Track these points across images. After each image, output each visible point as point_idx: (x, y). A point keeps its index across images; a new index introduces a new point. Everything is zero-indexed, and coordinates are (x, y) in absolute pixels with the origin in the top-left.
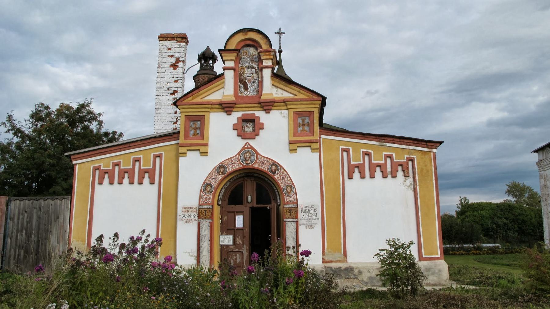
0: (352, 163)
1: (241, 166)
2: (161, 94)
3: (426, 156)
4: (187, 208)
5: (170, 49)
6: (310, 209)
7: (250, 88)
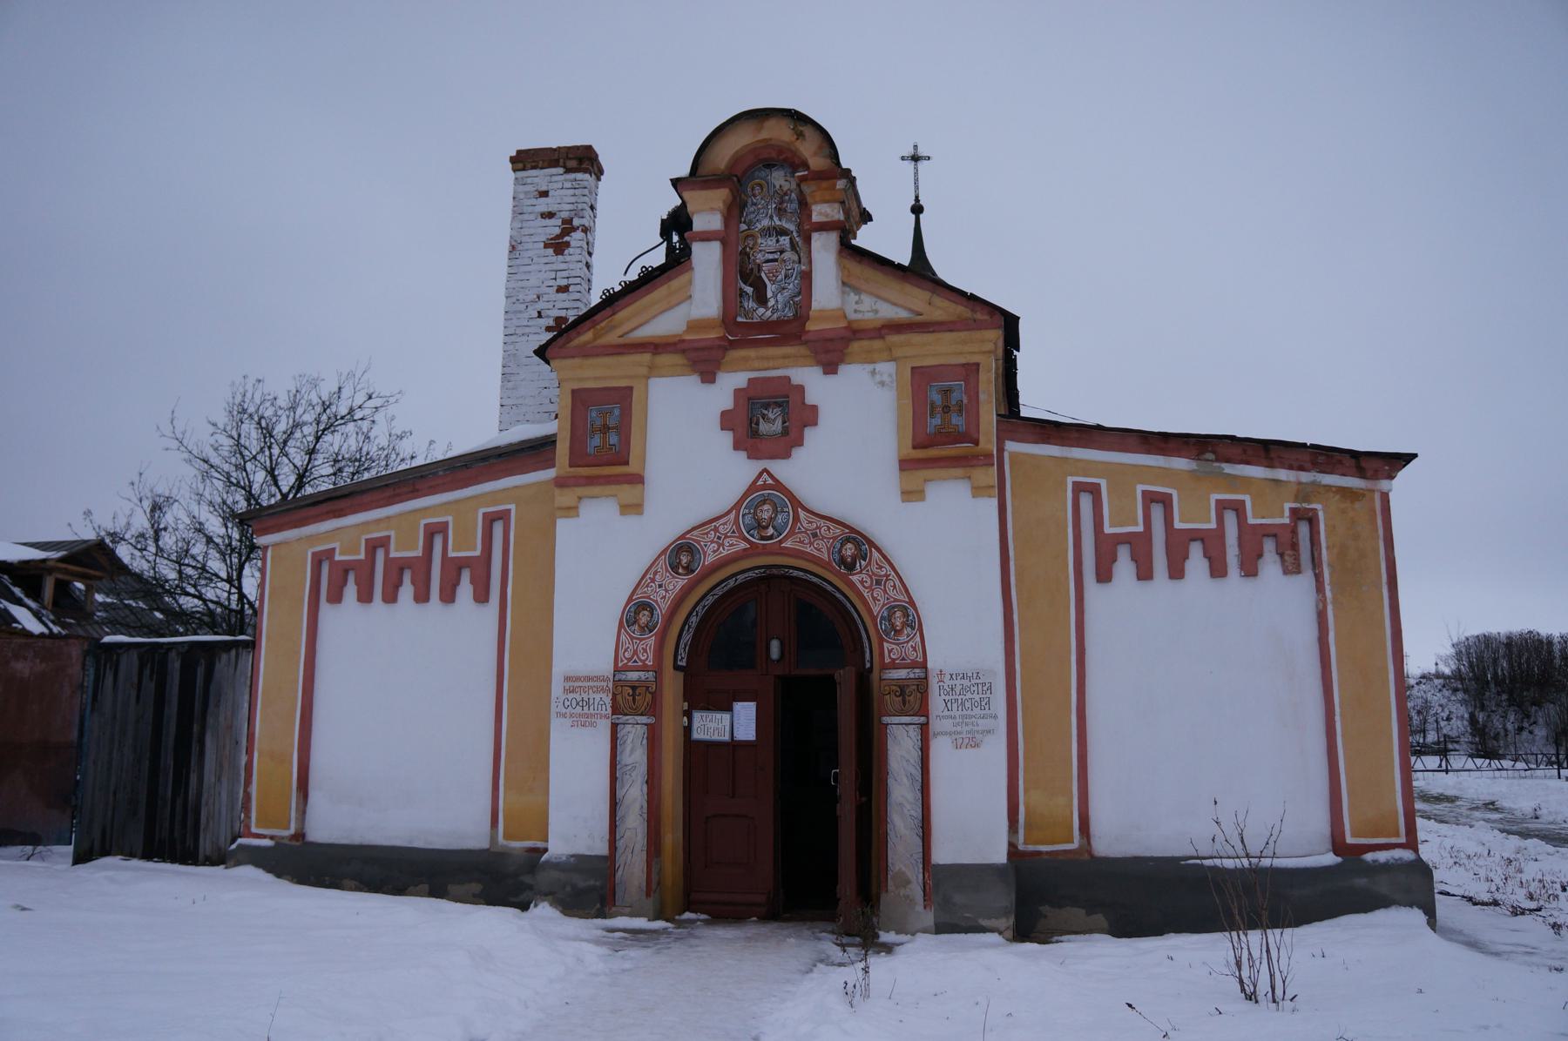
0: (1108, 530)
1: (744, 545)
2: (519, 331)
3: (1357, 505)
4: (578, 679)
5: (544, 194)
6: (966, 682)
7: (775, 296)
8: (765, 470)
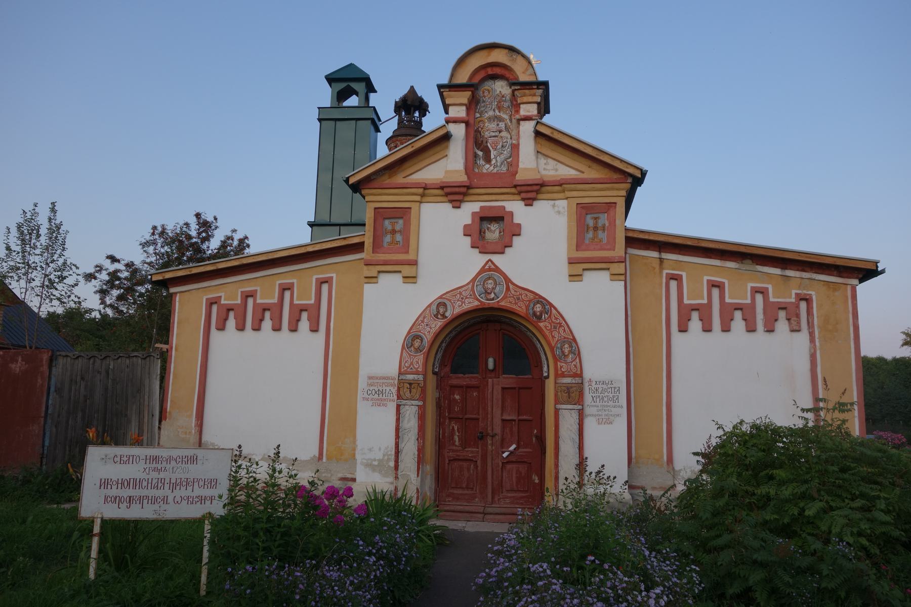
0: (686, 301)
3: (837, 293)
6: (605, 386)
7: (496, 158)
8: (490, 260)
